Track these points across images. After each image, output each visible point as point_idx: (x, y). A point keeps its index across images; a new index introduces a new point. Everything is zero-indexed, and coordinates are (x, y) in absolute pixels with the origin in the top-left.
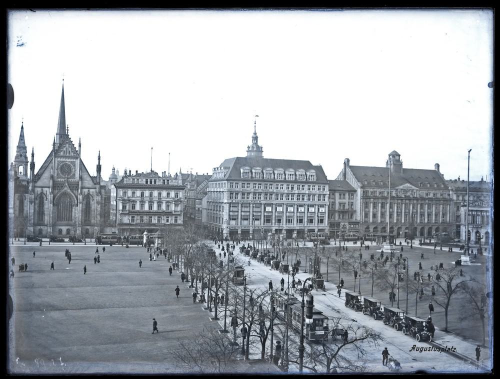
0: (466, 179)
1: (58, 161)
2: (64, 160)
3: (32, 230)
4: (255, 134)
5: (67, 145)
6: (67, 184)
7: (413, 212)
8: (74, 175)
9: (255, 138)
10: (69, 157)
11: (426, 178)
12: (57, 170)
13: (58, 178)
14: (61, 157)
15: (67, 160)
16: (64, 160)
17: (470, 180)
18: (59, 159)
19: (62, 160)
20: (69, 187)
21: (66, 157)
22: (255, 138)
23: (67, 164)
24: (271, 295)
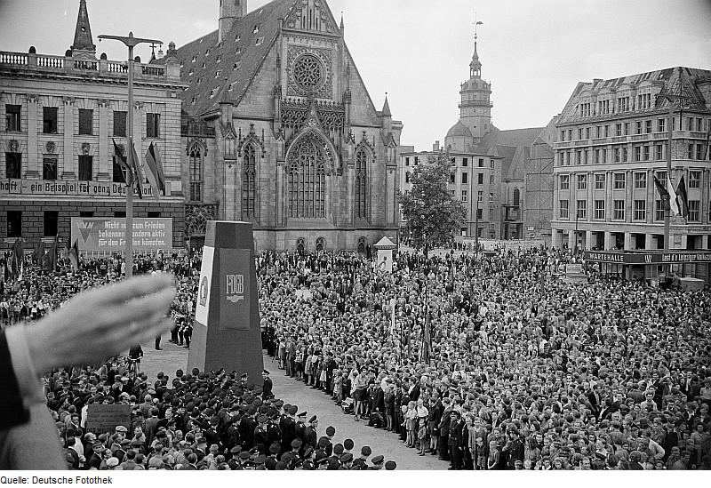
1: (290, 46)
4: (476, 57)
9: (476, 65)
15: (310, 43)
18: (291, 41)
22: (476, 65)
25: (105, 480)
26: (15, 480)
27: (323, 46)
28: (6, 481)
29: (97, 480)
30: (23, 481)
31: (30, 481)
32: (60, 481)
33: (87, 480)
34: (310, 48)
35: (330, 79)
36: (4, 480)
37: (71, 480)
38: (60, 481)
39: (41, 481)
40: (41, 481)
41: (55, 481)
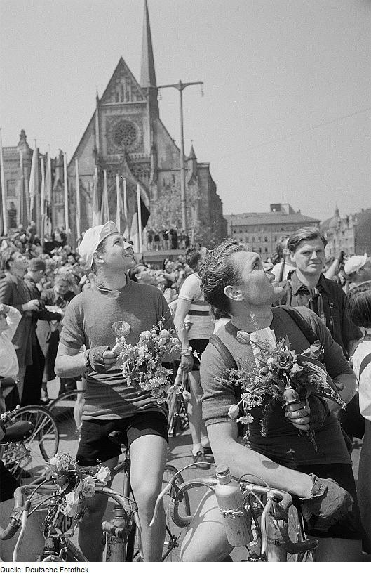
0: (158, 85)
1: (107, 117)
2: (118, 113)
3: (200, 300)
5: (123, 81)
6: (126, 165)
7: (67, 394)
8: (142, 143)
9: (23, 136)
10: (127, 106)
11: (266, 240)
12: (107, 136)
13: (108, 153)
14: (116, 107)
15: (124, 112)
16: (118, 113)
17: (161, 91)
18: (109, 113)
19: (114, 113)
20: (132, 170)
21: (122, 107)
22: (23, 136)
23: (125, 121)
24: (34, 246)
25: (83, 569)
26: (12, 569)
27: (135, 112)
28: (5, 571)
29: (76, 570)
30: (18, 570)
31: (24, 570)
32: (47, 570)
33: (68, 570)
34: (124, 116)
35: (142, 137)
36: (3, 570)
37: (56, 569)
38: (47, 570)
39: (32, 570)
40: (32, 570)
41: (43, 571)
